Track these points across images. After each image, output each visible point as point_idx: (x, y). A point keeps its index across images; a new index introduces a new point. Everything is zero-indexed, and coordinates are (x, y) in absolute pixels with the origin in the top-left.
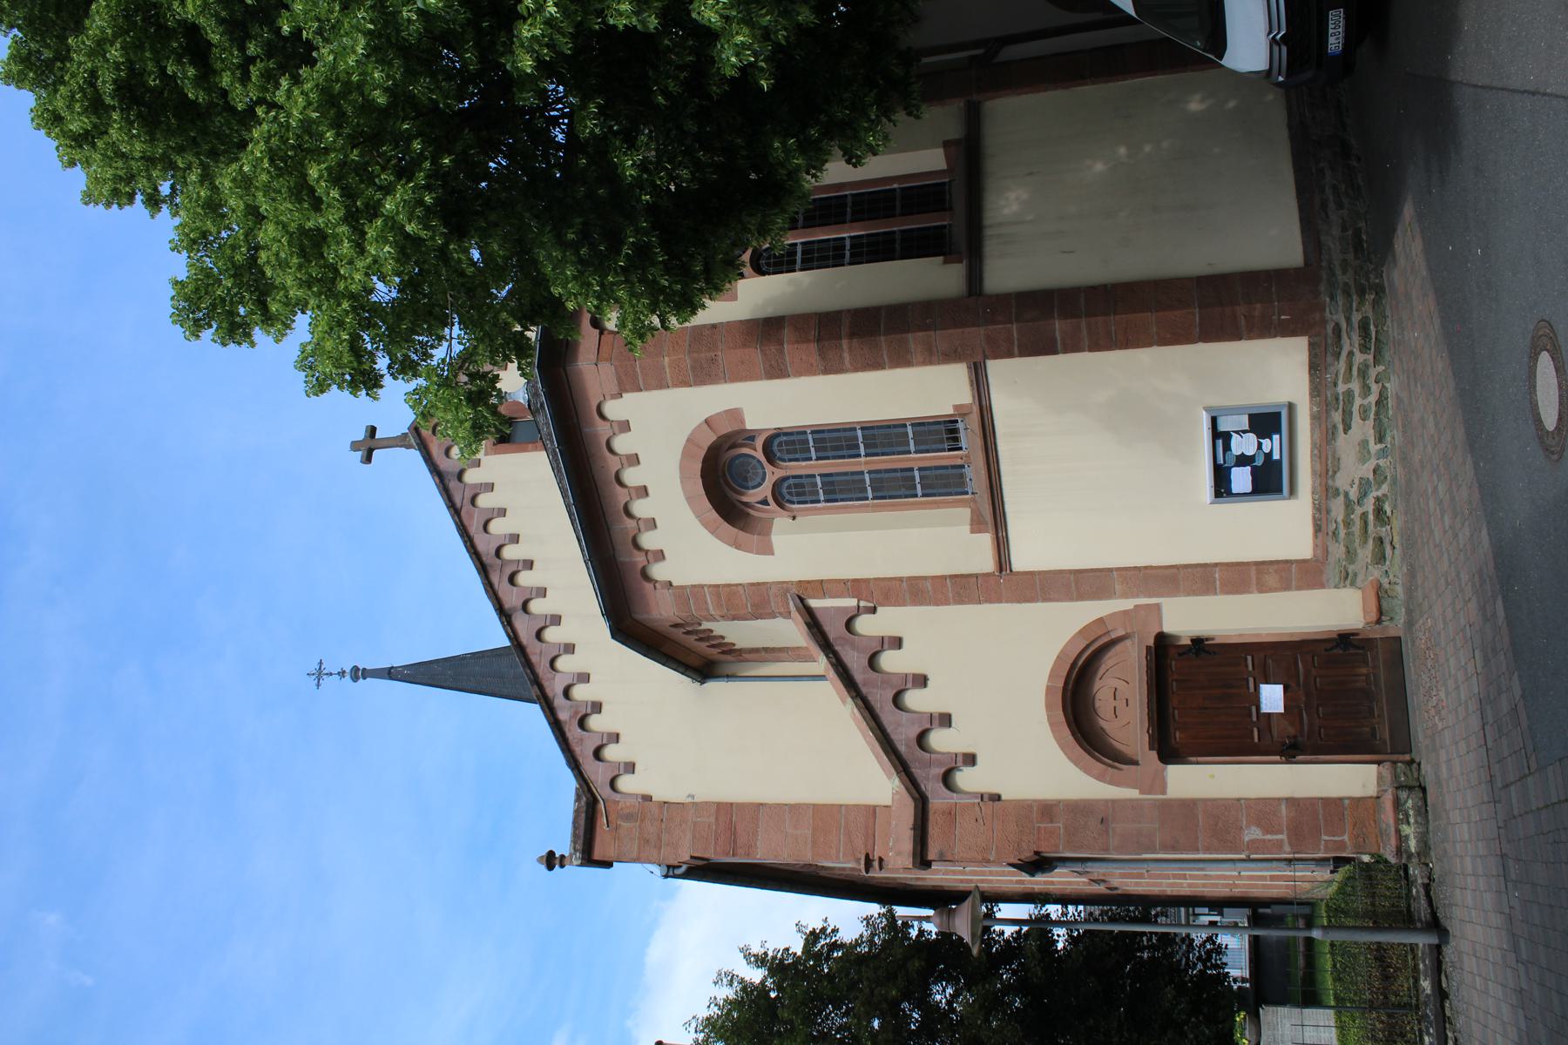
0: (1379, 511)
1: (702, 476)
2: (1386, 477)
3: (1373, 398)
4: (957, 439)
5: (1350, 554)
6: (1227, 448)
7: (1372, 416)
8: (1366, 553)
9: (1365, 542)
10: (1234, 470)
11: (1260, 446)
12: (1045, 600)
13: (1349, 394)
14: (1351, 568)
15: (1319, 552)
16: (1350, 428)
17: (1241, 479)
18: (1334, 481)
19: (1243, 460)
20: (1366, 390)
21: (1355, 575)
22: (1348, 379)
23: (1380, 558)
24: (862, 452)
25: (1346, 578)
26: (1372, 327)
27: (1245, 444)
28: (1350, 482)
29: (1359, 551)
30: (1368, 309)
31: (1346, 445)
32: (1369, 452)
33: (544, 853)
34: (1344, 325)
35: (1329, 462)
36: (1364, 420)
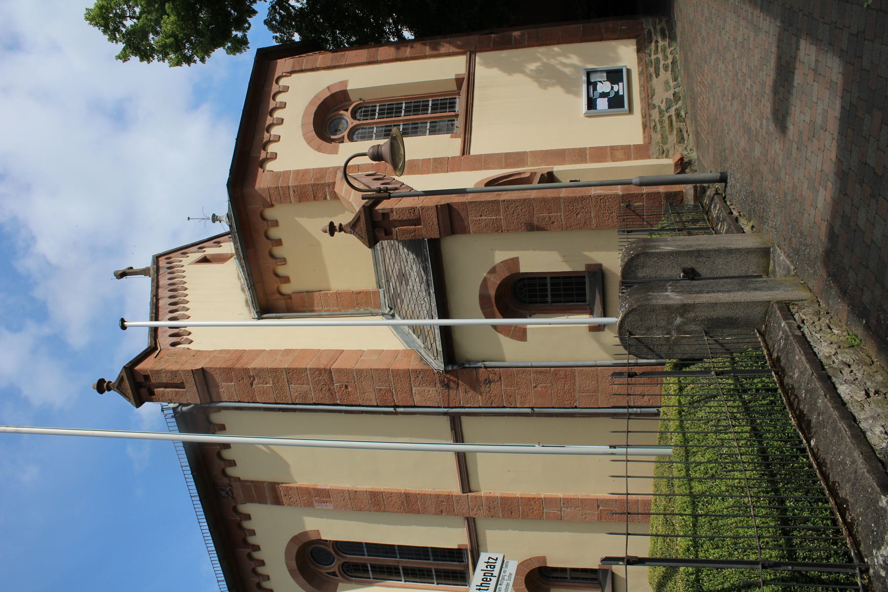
0: (678, 115)
1: (228, 185)
2: (680, 97)
3: (669, 61)
4: (454, 107)
5: (664, 140)
6: (595, 89)
7: (670, 69)
8: (673, 138)
9: (672, 131)
10: (598, 100)
11: (612, 88)
13: (657, 60)
14: (665, 147)
15: (647, 140)
16: (659, 75)
17: (602, 103)
18: (652, 100)
19: (603, 95)
20: (666, 58)
21: (668, 151)
23: (681, 140)
25: (663, 152)
26: (667, 32)
27: (604, 87)
28: (661, 101)
29: (669, 137)
30: (664, 24)
31: (657, 83)
32: (670, 86)
34: (653, 30)
35: (649, 91)
36: (666, 71)
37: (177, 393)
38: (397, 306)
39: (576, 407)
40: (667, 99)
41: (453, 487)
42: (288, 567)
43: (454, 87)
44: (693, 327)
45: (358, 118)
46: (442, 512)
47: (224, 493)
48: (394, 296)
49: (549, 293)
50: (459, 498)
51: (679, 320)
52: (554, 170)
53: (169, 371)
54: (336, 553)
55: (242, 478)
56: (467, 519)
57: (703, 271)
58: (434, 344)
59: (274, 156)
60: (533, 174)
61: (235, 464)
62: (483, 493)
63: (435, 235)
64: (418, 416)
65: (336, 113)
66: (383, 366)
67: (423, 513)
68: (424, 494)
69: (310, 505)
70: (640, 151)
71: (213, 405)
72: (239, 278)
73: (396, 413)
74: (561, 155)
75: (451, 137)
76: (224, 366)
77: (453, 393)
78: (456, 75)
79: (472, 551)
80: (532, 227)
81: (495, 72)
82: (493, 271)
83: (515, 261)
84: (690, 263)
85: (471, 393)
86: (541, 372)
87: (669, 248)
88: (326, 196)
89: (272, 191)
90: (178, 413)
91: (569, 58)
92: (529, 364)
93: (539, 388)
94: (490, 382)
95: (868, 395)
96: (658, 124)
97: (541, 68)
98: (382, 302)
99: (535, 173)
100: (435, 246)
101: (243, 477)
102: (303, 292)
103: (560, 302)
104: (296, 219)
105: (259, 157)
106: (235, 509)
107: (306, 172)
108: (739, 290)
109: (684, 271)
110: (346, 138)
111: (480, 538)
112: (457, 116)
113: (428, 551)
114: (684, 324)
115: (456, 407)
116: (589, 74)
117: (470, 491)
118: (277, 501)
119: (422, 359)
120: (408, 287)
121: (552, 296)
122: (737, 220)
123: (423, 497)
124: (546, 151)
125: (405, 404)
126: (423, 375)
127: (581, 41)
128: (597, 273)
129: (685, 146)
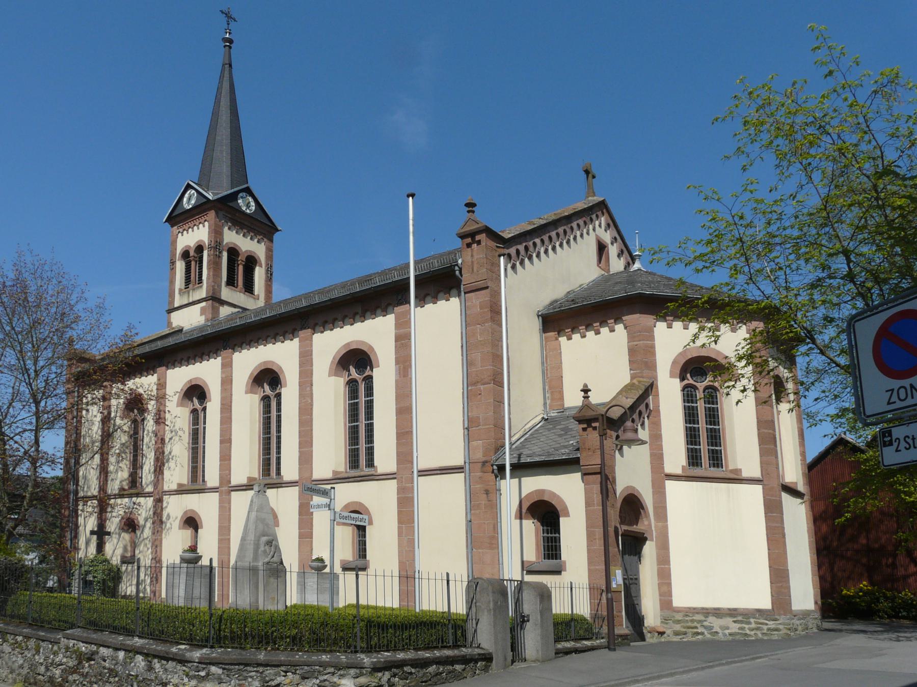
0: (698, 634)
3: (748, 632)
4: (714, 466)
5: (678, 622)
7: (740, 631)
8: (678, 627)
9: (684, 628)
13: (750, 623)
20: (752, 630)
21: (667, 623)
23: (677, 633)
25: (665, 620)
33: (589, 387)
38: (548, 424)
40: (713, 627)
42: (352, 342)
47: (400, 297)
75: (683, 466)
110: (686, 382)
113: (371, 443)
124: (668, 537)
127: (770, 567)
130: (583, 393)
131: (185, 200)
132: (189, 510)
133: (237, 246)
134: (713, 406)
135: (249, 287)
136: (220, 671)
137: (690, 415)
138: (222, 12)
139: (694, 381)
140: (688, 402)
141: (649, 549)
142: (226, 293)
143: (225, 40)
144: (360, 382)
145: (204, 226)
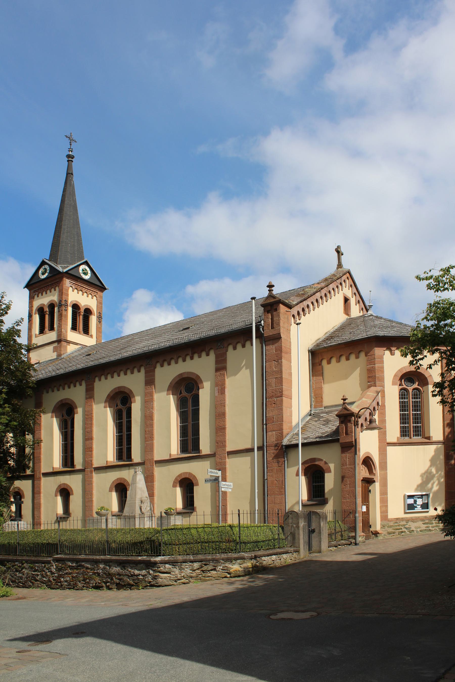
0: (402, 532)
3: (431, 528)
4: (416, 436)
6: (418, 498)
8: (390, 530)
9: (394, 530)
12: (379, 454)
13: (432, 524)
14: (386, 527)
17: (411, 501)
19: (415, 502)
20: (433, 527)
21: (384, 528)
22: (436, 523)
23: (389, 533)
24: (414, 412)
31: (420, 524)
33: (273, 284)
37: (269, 325)
38: (314, 418)
39: (267, 496)
40: (411, 527)
41: (228, 449)
43: (426, 436)
44: (293, 529)
45: (414, 391)
46: (217, 443)
47: (219, 344)
48: (319, 416)
49: (317, 484)
50: (225, 450)
51: (295, 526)
52: (376, 483)
53: (279, 321)
54: (192, 395)
55: (227, 353)
56: (215, 454)
57: (314, 535)
58: (294, 440)
59: (392, 354)
60: (374, 475)
61: (234, 350)
62: (227, 460)
63: (341, 441)
64: (262, 433)
65: (417, 380)
66: (284, 420)
67: (216, 435)
68: (225, 436)
69: (217, 385)
70: (384, 516)
71: (264, 342)
72: (333, 328)
73: (263, 424)
74: (384, 485)
75: (398, 437)
76: (283, 347)
77: (273, 448)
78: (432, 437)
79: (199, 455)
80: (343, 478)
81: (432, 453)
82: (326, 463)
83: (330, 471)
84: (317, 531)
85: (273, 455)
86: (283, 482)
87: (322, 525)
88: (370, 382)
89: (373, 356)
90: (259, 326)
91: (437, 485)
92: (286, 478)
93: (275, 482)
94: (278, 463)
95: (273, 561)
96: (398, 524)
97: (432, 474)
98: (317, 409)
99: (375, 475)
100: (338, 440)
101: (228, 354)
102: (322, 371)
103: (313, 488)
104: (359, 368)
105: (392, 347)
106: (211, 349)
107: (383, 372)
108: (304, 541)
109: (314, 529)
110: (401, 387)
111: (206, 459)
112: (411, 438)
114: (294, 527)
115: (266, 449)
116: (427, 495)
117: (228, 455)
118: (217, 370)
119: (288, 434)
120: (322, 425)
121: (316, 485)
122: (336, 547)
123: (224, 435)
124: (387, 479)
125: (267, 428)
126: (281, 436)
128: (324, 502)
129: (386, 535)
130: (343, 400)
131: (40, 272)
132: (63, 484)
133: (79, 302)
134: (417, 400)
135: (86, 331)
136: (170, 566)
137: (403, 407)
138: (67, 137)
139: (407, 386)
140: (402, 399)
141: (376, 487)
142: (72, 336)
143: (68, 156)
144: (188, 398)
145: (55, 290)
